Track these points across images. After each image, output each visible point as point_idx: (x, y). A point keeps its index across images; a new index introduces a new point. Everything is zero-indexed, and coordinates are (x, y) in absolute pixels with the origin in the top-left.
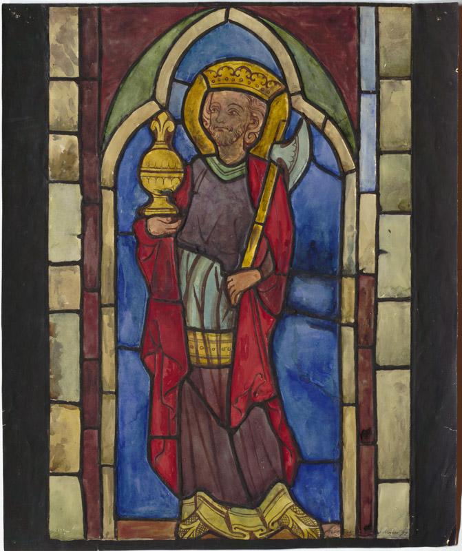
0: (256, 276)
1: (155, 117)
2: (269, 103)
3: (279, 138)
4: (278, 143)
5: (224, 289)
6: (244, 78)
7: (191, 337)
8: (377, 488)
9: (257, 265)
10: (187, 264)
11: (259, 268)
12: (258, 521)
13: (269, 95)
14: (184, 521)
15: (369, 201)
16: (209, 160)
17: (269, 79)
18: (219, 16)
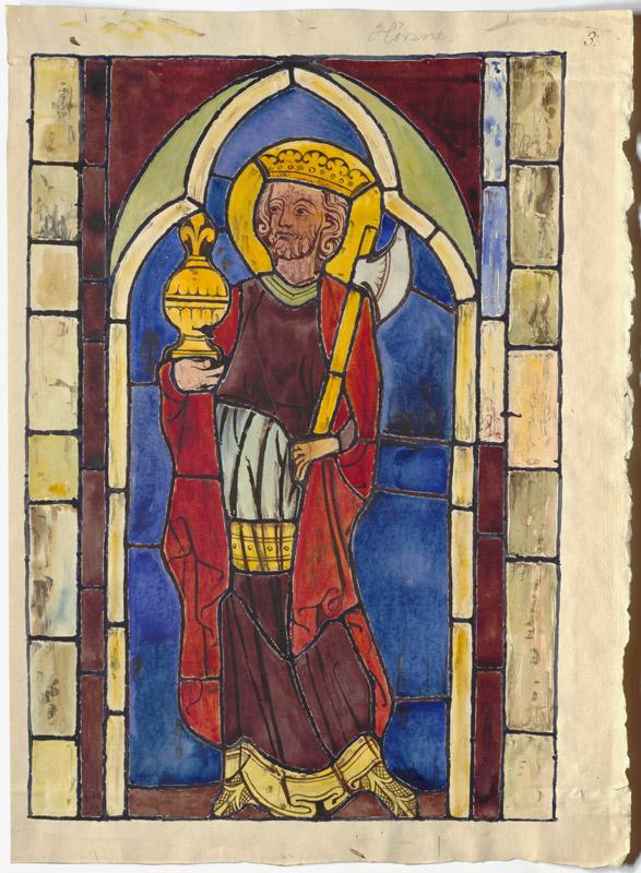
0: (332, 445)
1: (186, 221)
2: (350, 201)
3: (366, 250)
4: (363, 257)
5: (286, 464)
6: (337, 173)
7: (235, 529)
8: (78, 631)
9: (335, 429)
10: (235, 433)
11: (337, 436)
12: (334, 781)
13: (352, 189)
14: (229, 780)
15: (493, 333)
16: (264, 279)
17: (351, 167)
18: (277, 82)
